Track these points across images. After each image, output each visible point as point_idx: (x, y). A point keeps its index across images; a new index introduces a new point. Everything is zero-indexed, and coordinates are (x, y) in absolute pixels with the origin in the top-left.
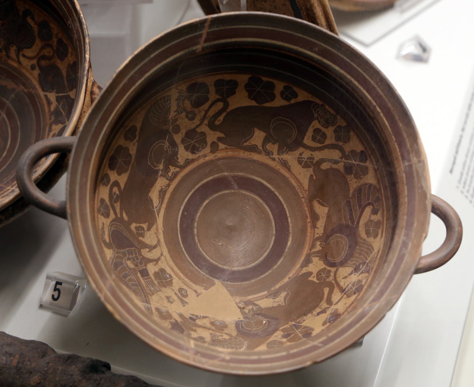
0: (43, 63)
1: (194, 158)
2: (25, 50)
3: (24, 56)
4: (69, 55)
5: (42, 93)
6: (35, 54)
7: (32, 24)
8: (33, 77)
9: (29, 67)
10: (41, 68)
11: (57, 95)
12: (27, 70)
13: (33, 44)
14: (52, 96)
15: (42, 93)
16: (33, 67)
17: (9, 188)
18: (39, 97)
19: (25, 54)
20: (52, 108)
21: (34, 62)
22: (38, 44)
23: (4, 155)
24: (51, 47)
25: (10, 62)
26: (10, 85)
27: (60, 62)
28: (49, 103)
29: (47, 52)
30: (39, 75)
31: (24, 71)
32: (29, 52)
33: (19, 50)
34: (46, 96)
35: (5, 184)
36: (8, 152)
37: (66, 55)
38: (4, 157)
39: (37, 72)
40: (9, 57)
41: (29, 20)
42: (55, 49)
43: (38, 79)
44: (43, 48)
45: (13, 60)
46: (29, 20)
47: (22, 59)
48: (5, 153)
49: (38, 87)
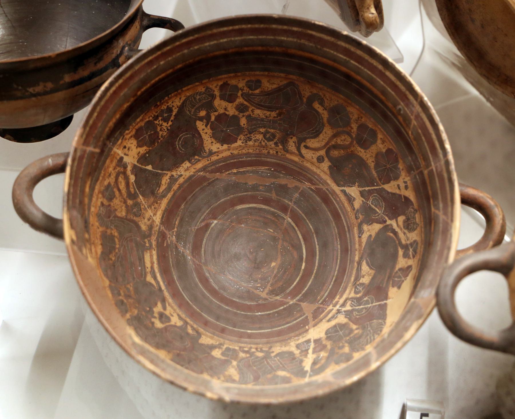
0: (335, 153)
1: (363, 236)
2: (308, 140)
3: (306, 147)
4: (379, 141)
5: (337, 189)
6: (323, 144)
7: (320, 109)
8: (322, 171)
9: (315, 160)
10: (330, 159)
11: (361, 189)
12: (312, 163)
13: (321, 132)
14: (354, 191)
15: (337, 189)
16: (320, 160)
17: (331, 307)
18: (334, 193)
19: (308, 145)
20: (357, 204)
21: (322, 153)
22: (327, 132)
23: (303, 267)
24: (349, 134)
25: (288, 156)
26: (291, 183)
27: (363, 151)
28: (350, 199)
29: (343, 140)
30: (330, 168)
31: (308, 165)
32: (313, 143)
33: (300, 141)
34: (344, 192)
35: (322, 303)
36: (306, 262)
37: (374, 142)
38: (304, 270)
39: (326, 165)
40: (287, 151)
41: (316, 105)
42: (354, 136)
43: (328, 172)
44: (334, 136)
45: (292, 153)
46: (316, 105)
47: (304, 151)
48: (304, 264)
49: (330, 181)
